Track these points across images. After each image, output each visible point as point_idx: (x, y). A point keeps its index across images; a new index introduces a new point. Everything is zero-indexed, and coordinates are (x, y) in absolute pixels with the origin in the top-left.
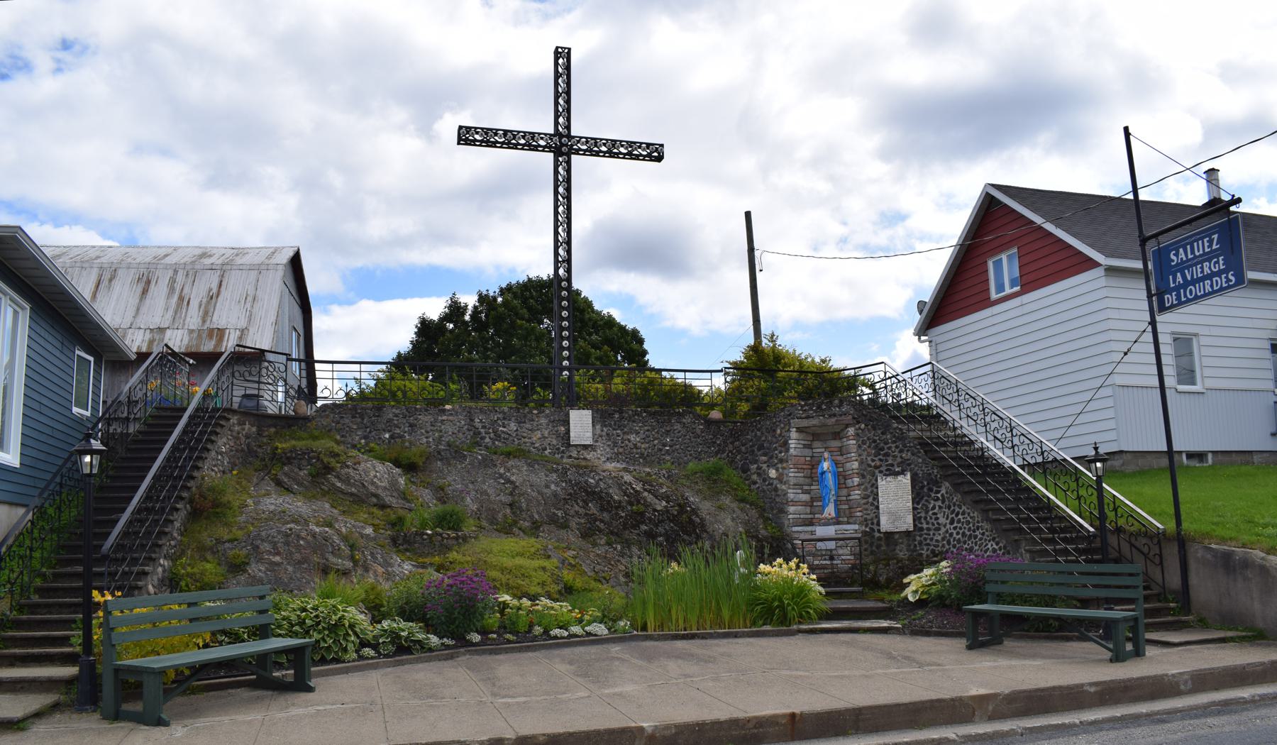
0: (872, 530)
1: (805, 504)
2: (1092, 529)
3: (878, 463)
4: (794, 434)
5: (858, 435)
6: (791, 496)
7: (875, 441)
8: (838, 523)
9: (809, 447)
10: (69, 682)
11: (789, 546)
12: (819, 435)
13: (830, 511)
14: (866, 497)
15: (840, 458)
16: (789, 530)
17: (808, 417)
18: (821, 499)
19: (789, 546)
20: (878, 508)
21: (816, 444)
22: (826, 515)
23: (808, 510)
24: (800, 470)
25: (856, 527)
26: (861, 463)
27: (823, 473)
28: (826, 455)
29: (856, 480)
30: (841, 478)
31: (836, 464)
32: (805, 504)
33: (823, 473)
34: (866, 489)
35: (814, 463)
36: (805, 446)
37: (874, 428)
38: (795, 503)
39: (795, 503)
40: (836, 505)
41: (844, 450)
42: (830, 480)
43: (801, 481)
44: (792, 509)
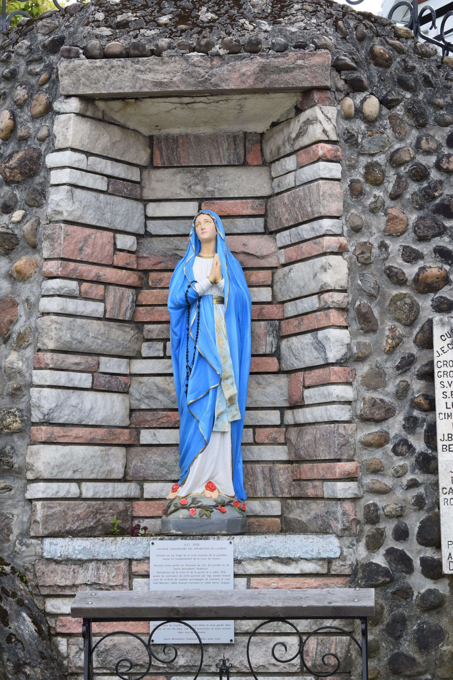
0: (401, 560)
1: (103, 437)
2: (24, 614)
3: (434, 268)
4: (69, 127)
5: (350, 139)
6: (44, 400)
7: (420, 174)
8: (246, 527)
9: (129, 190)
10: (365, 617)
11: (26, 626)
12: (173, 141)
13: (213, 470)
14: (376, 415)
15: (260, 245)
16: (27, 553)
17: (133, 53)
18: (174, 415)
19: (26, 626)
20: (428, 464)
21: (163, 182)
22: (193, 486)
23: (116, 461)
24: (89, 285)
25: (329, 546)
26: (361, 262)
27: (191, 303)
28: (206, 225)
29: (337, 341)
30: (270, 327)
31: (249, 266)
32: (103, 437)
33: (191, 303)
34: (376, 380)
35: (147, 268)
36: (118, 187)
37: (419, 119)
38: (59, 430)
39: (59, 430)
40: (238, 446)
41: (282, 211)
42: (218, 332)
43: (93, 334)
44: (44, 458)
